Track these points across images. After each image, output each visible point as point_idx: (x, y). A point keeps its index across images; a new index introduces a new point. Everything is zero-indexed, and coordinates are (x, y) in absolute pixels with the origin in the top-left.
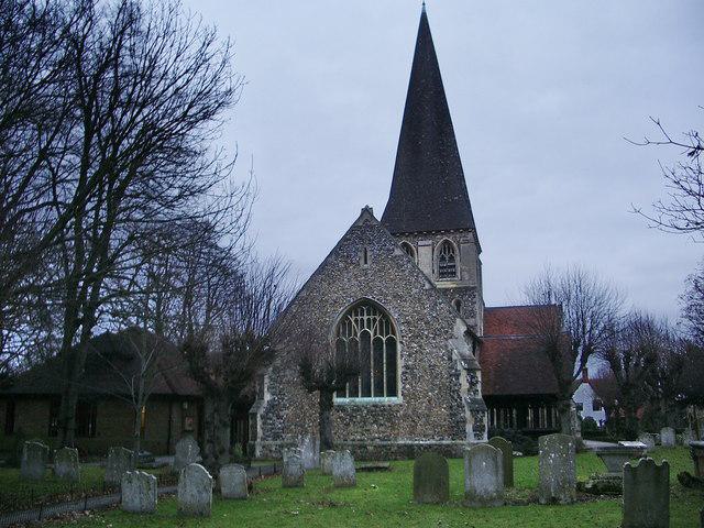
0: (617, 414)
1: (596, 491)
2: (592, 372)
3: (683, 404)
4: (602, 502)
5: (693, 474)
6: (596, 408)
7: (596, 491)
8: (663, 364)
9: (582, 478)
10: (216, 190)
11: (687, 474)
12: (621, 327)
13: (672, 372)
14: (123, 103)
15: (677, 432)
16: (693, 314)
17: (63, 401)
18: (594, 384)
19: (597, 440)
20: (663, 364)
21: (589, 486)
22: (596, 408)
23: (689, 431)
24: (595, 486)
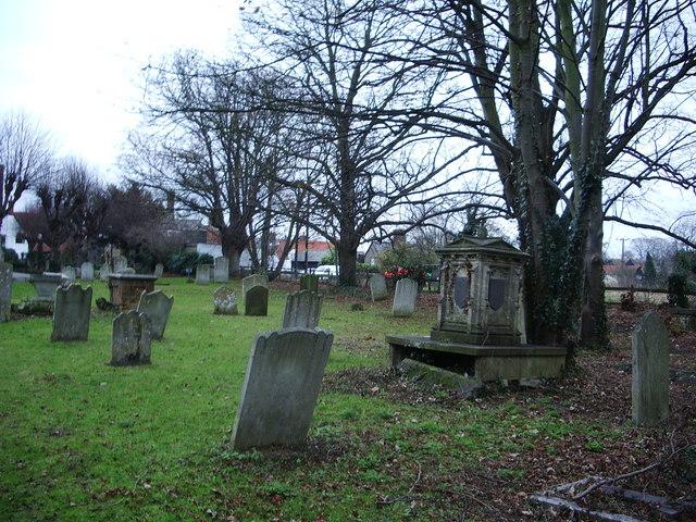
0: (40, 247)
1: (28, 312)
2: (19, 207)
3: (103, 243)
4: (33, 321)
5: (108, 300)
6: (19, 240)
7: (28, 312)
8: (90, 204)
9: (16, 301)
10: (15, 120)
11: (104, 300)
12: (56, 169)
13: (97, 212)
14: (285, 212)
15: (96, 268)
16: (122, 163)
17: (502, 408)
18: (19, 217)
19: (21, 272)
20: (90, 204)
21: (22, 308)
22: (19, 240)
23: (106, 266)
24: (26, 308)
